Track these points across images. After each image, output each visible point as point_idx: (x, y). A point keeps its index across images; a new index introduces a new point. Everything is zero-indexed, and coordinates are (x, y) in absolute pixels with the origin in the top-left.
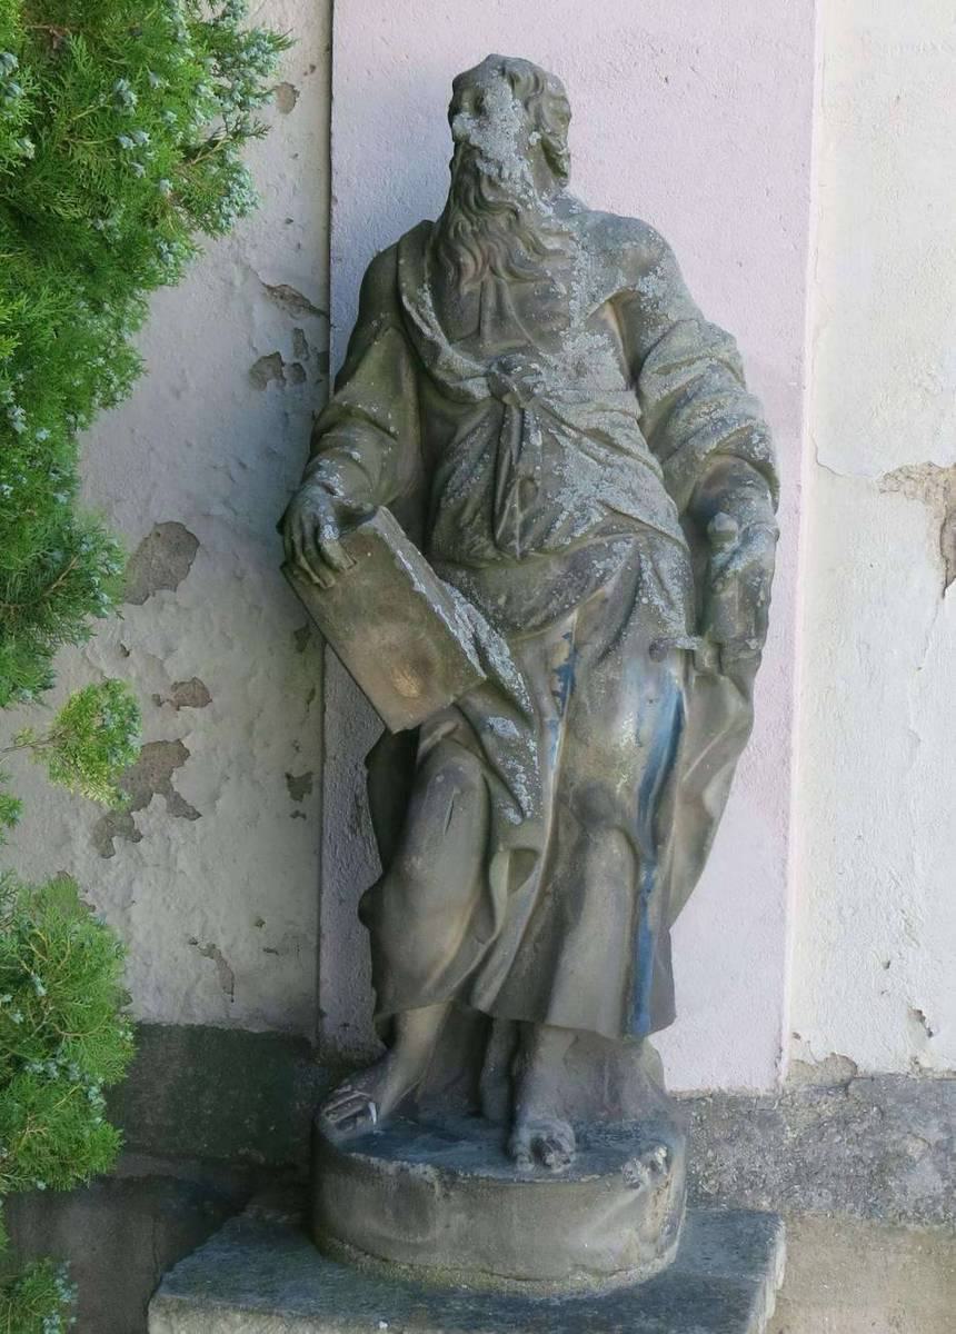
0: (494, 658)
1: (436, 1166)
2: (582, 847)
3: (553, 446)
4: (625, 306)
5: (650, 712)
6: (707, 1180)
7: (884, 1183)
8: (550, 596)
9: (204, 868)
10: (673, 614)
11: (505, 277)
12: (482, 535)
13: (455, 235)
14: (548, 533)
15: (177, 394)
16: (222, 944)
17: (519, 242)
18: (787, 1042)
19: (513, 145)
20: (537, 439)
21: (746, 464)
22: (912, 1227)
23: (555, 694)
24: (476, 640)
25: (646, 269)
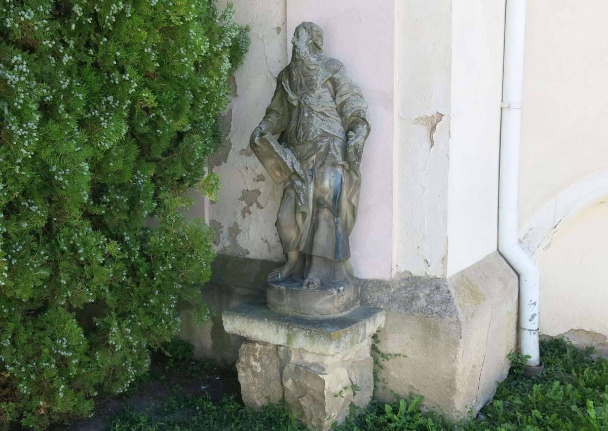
0: (295, 167)
1: (285, 286)
2: (318, 212)
3: (310, 116)
5: (333, 180)
6: (370, 300)
7: (412, 302)
8: (308, 152)
9: (265, 221)
10: (338, 156)
11: (302, 76)
14: (307, 137)
15: (257, 105)
16: (269, 240)
17: (305, 67)
18: (394, 266)
19: (304, 44)
20: (306, 115)
21: (360, 119)
22: (416, 314)
23: (310, 175)
24: (292, 163)
25: (336, 72)
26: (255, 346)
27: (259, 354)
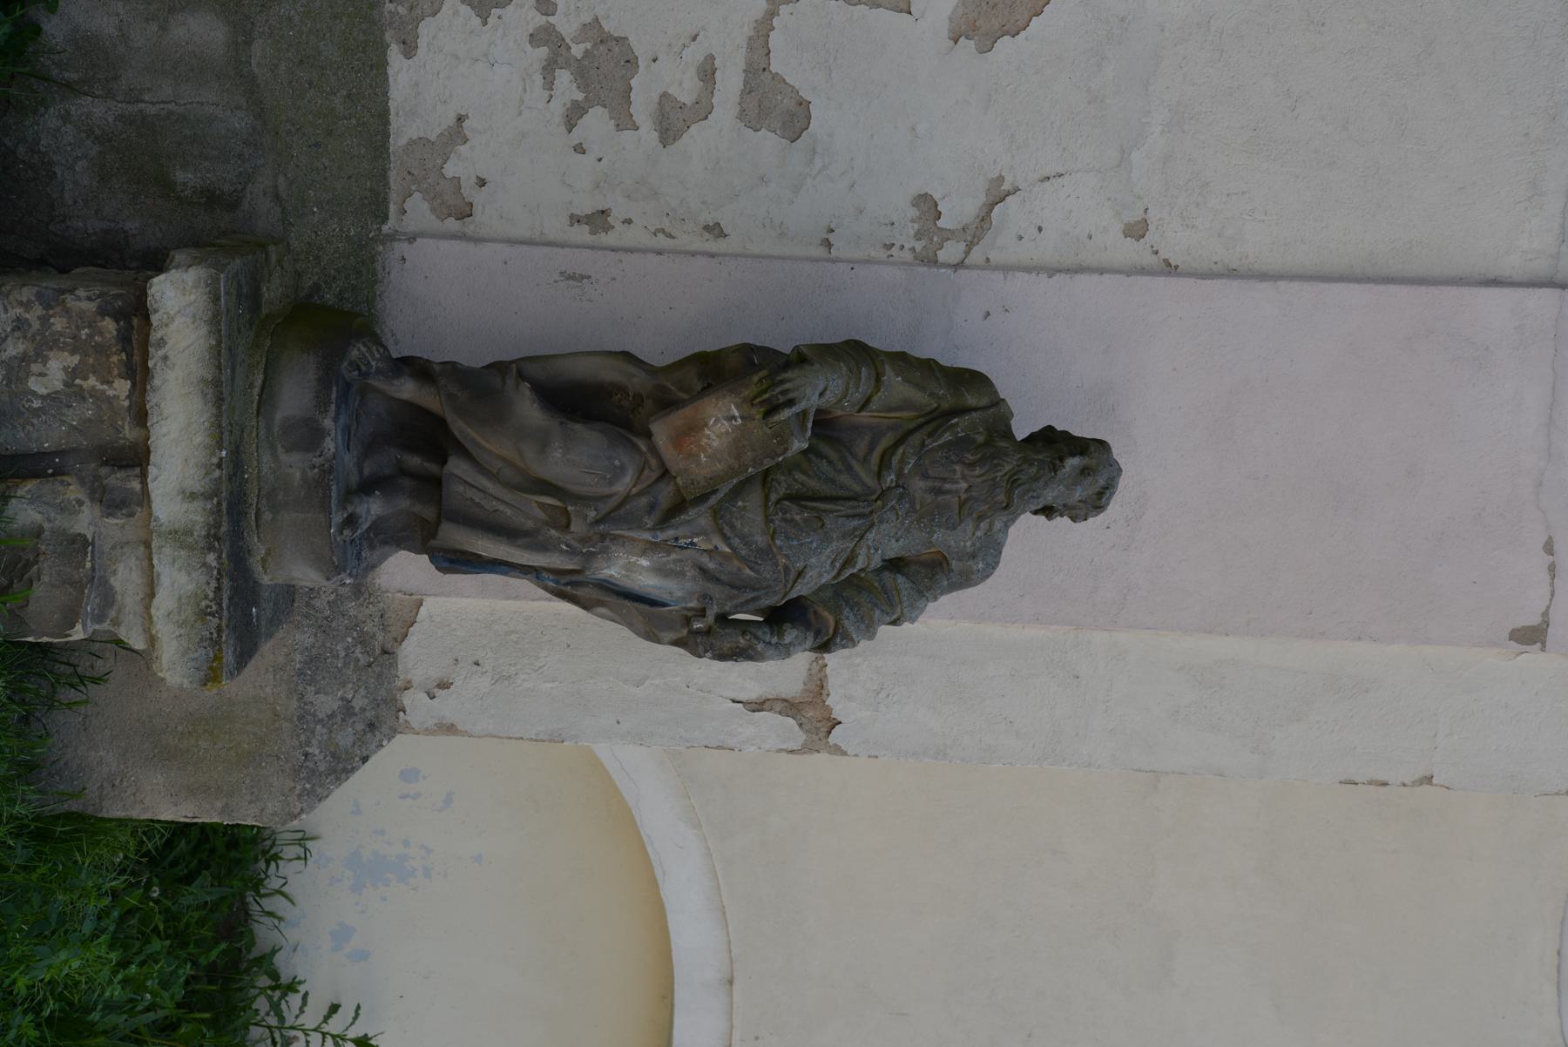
4: (940, 564)
12: (787, 489)
13: (995, 464)
26: (120, 376)
27: (93, 392)
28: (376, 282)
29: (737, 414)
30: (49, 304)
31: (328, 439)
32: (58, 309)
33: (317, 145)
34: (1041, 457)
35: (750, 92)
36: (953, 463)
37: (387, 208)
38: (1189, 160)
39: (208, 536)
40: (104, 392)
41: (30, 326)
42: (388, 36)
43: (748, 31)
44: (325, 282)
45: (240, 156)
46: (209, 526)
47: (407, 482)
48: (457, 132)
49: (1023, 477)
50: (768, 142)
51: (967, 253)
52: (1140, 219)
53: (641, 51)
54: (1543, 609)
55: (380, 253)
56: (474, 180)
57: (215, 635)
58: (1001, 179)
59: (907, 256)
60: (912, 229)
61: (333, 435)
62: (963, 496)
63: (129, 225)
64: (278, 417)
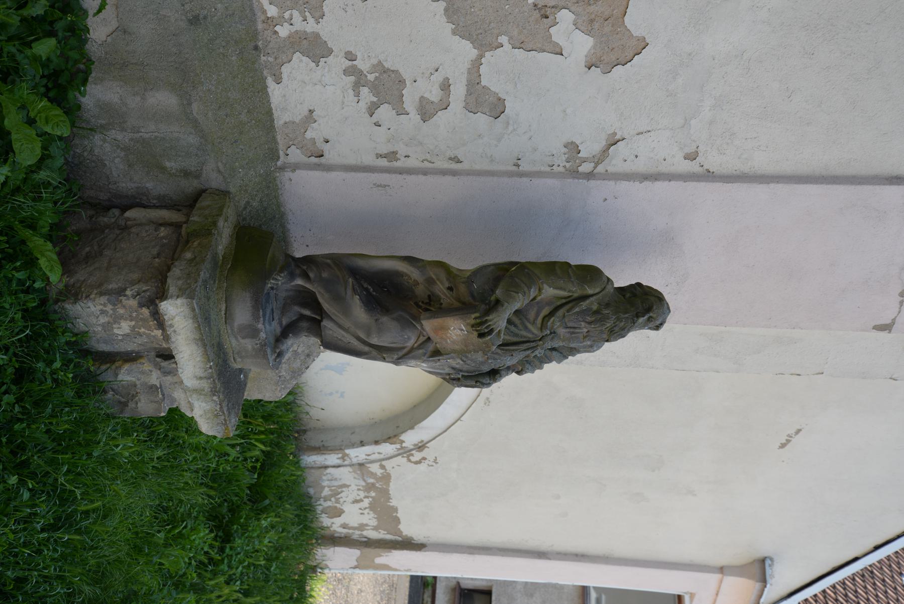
28: (278, 189)
29: (464, 329)
30: (114, 304)
31: (262, 333)
32: (119, 305)
33: (236, 141)
34: (626, 316)
35: (470, 95)
36: (580, 321)
37: (278, 154)
38: (724, 123)
39: (211, 391)
40: (150, 334)
41: (108, 312)
42: (265, 72)
43: (467, 65)
44: (252, 199)
45: (196, 155)
46: (212, 388)
47: (304, 324)
48: (310, 117)
49: (616, 329)
50: (482, 120)
51: (595, 168)
52: (694, 151)
53: (407, 75)
54: (893, 317)
55: (278, 177)
56: (322, 140)
57: (224, 422)
58: (615, 134)
59: (561, 169)
60: (564, 158)
61: (264, 331)
62: (585, 334)
63: (147, 185)
64: (236, 324)
